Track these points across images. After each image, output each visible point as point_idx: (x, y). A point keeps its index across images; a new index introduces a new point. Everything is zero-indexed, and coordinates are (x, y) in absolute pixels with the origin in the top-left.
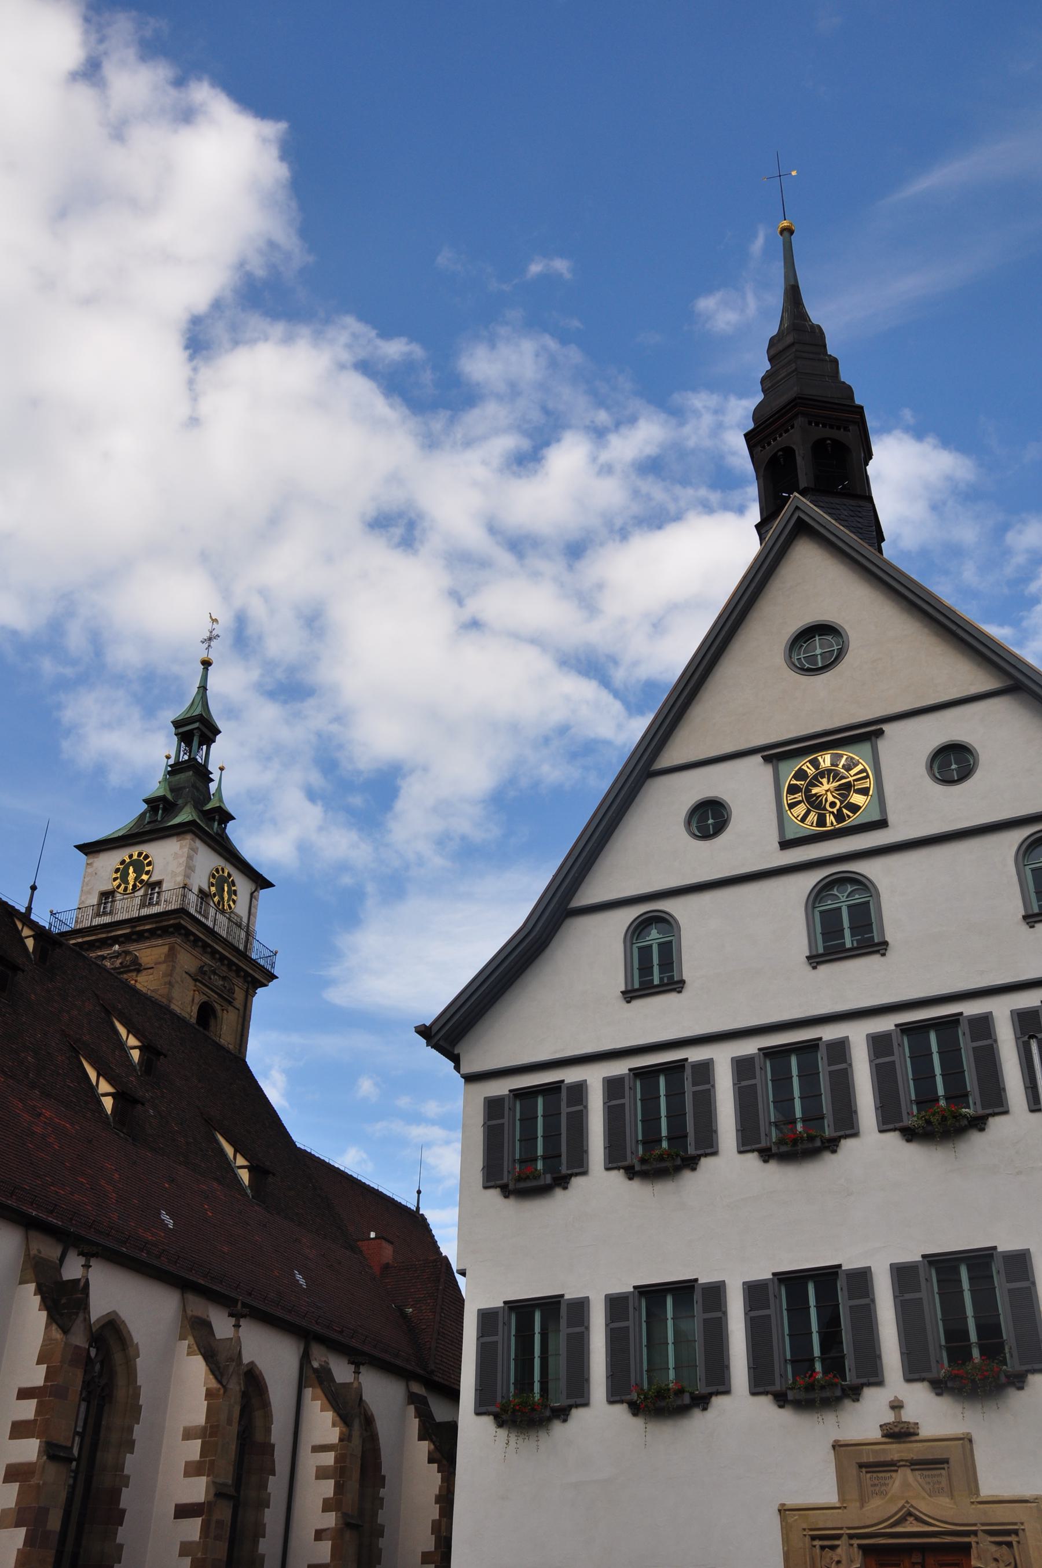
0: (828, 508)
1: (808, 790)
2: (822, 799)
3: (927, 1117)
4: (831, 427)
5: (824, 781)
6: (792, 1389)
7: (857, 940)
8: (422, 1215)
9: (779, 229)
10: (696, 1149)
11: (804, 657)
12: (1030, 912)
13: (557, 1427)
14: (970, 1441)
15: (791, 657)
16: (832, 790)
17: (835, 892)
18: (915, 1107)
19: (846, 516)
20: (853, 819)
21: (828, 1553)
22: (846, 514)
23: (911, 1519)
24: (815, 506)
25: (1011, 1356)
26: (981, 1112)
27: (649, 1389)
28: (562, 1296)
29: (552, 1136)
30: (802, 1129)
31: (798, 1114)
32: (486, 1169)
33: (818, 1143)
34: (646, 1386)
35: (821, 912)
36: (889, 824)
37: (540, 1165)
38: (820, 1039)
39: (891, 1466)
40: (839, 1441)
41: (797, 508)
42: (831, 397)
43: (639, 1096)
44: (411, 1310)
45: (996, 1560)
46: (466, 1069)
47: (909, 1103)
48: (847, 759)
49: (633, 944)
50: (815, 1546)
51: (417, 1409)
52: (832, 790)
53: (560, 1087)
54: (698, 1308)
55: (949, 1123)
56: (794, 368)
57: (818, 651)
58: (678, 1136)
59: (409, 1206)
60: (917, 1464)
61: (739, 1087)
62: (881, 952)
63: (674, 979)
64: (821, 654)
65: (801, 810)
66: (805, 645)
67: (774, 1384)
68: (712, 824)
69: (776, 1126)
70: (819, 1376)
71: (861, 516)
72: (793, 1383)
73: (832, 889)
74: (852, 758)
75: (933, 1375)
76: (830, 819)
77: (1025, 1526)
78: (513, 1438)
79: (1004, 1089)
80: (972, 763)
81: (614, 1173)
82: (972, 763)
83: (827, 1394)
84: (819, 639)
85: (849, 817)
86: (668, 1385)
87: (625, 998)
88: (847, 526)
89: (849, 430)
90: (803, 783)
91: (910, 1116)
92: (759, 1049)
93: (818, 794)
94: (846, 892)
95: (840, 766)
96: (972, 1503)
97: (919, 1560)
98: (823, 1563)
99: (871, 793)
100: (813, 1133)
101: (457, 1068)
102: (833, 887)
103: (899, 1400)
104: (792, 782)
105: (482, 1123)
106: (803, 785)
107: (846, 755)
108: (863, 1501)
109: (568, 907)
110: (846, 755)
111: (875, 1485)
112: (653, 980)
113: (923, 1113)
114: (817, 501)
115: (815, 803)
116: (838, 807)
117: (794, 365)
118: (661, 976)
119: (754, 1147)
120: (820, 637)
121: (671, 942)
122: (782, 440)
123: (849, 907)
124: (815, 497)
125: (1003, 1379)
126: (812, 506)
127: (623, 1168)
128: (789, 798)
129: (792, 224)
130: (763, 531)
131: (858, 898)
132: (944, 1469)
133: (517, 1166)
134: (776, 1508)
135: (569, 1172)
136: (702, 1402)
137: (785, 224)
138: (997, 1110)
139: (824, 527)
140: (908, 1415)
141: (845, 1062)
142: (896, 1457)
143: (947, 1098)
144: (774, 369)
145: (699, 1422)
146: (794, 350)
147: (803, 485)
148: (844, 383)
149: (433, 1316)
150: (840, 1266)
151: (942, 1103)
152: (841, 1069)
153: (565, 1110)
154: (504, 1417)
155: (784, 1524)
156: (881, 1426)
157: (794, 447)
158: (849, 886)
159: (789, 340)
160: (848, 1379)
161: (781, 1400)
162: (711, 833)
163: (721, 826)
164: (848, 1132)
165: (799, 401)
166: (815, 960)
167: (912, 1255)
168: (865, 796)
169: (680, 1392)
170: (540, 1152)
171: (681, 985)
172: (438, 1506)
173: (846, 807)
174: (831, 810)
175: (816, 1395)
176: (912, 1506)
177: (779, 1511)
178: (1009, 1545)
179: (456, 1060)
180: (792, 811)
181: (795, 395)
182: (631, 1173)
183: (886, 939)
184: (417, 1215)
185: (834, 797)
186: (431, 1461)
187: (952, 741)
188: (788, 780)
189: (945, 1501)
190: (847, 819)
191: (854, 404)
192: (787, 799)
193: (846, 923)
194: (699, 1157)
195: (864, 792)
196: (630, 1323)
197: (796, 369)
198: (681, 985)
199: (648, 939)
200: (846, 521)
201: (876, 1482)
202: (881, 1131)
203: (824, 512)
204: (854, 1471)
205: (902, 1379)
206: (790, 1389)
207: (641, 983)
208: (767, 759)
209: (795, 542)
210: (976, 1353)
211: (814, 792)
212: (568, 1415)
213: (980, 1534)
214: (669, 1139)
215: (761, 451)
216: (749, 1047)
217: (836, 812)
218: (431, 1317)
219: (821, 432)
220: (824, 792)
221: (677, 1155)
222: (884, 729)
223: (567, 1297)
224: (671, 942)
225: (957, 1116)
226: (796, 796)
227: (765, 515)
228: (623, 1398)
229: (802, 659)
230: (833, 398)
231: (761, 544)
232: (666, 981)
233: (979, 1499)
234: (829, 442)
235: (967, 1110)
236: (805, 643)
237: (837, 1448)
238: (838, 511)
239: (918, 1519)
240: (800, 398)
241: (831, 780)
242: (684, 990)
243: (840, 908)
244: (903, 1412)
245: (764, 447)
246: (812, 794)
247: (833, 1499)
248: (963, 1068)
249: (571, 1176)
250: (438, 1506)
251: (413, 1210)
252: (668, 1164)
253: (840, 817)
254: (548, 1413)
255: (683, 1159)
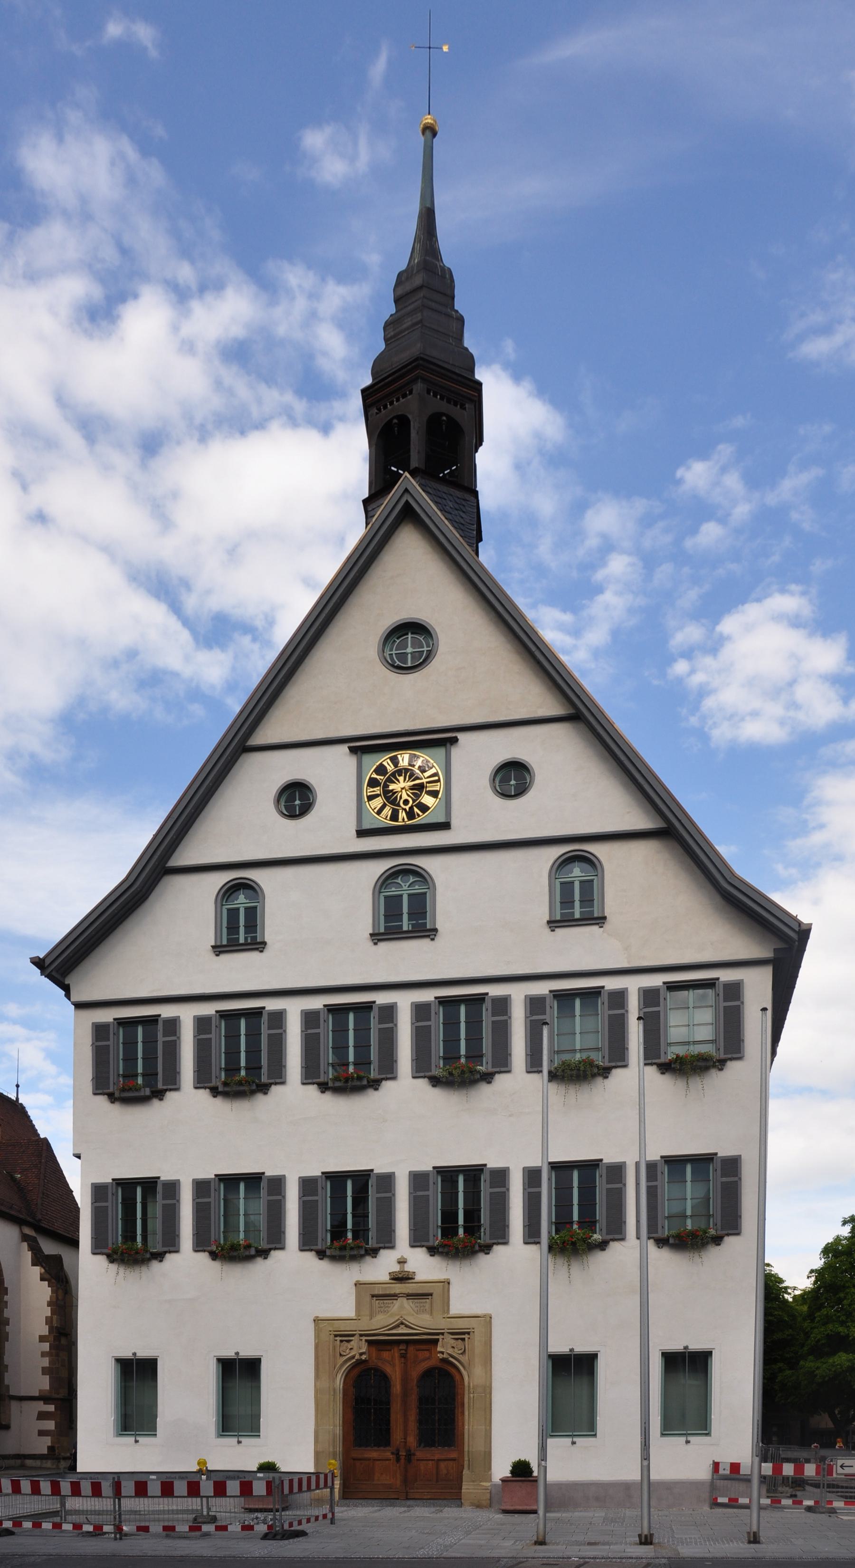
0: (435, 496)
1: (386, 786)
2: (397, 796)
3: (450, 1070)
4: (449, 401)
5: (401, 779)
6: (330, 1248)
7: (412, 924)
8: (21, 1104)
9: (422, 126)
10: (268, 1079)
11: (396, 654)
12: (553, 919)
13: (155, 1265)
14: (449, 1283)
15: (383, 652)
16: (407, 788)
17: (399, 881)
18: (441, 1062)
19: (451, 507)
20: (422, 818)
21: (345, 1344)
22: (452, 506)
23: (403, 1326)
24: (424, 491)
25: (485, 1234)
26: (491, 1070)
27: (225, 1244)
28: (159, 1178)
29: (151, 1059)
30: (353, 1071)
31: (351, 1058)
32: (95, 1080)
33: (365, 1082)
34: (222, 1242)
35: (386, 897)
36: (452, 827)
37: (140, 1080)
38: (374, 1002)
39: (395, 1296)
40: (359, 1281)
41: (406, 490)
42: (452, 365)
43: (223, 1033)
44: (19, 1176)
45: (453, 1347)
46: (76, 997)
47: (437, 1058)
48: (423, 761)
49: (222, 905)
50: (336, 1340)
51: (29, 1245)
52: (407, 788)
53: (157, 1020)
54: (263, 1192)
55: (466, 1076)
56: (419, 318)
57: (409, 650)
58: (254, 1067)
59: (10, 1096)
60: (409, 1296)
61: (306, 1034)
62: (432, 937)
63: (257, 939)
64: (411, 653)
65: (378, 803)
66: (398, 641)
67: (317, 1245)
68: (298, 805)
69: (333, 1066)
70: (350, 1241)
71: (464, 510)
72: (331, 1245)
73: (397, 878)
74: (428, 761)
75: (430, 1244)
76: (402, 815)
77: (475, 1330)
78: (122, 1270)
79: (510, 1055)
80: (528, 781)
81: (202, 1091)
82: (528, 781)
83: (355, 1252)
84: (412, 637)
85: (419, 816)
86: (239, 1242)
87: (215, 952)
88: (451, 520)
89: (465, 409)
90: (382, 778)
91: (437, 1069)
92: (325, 1006)
93: (394, 791)
94: (408, 882)
95: (417, 767)
96: (444, 1318)
97: (404, 1348)
98: (341, 1349)
99: (440, 796)
100: (362, 1074)
101: (68, 995)
102: (398, 877)
103: (404, 1258)
104: (372, 776)
105: (91, 1043)
106: (382, 780)
107: (423, 757)
108: (371, 1316)
109: (167, 865)
110: (423, 757)
111: (381, 1307)
112: (238, 938)
113: (448, 1067)
114: (425, 486)
115: (391, 798)
116: (410, 805)
117: (419, 314)
118: (246, 935)
119: (315, 1081)
120: (413, 636)
121: (256, 907)
122: (398, 406)
123: (409, 895)
124: (423, 480)
125: (477, 1248)
126: (421, 491)
127: (209, 1088)
128: (368, 791)
129: (435, 122)
130: (370, 508)
131: (418, 889)
132: (428, 1299)
133: (121, 1079)
134: (312, 1319)
135: (165, 1087)
136: (264, 1253)
137: (428, 120)
138: (503, 1069)
139: (430, 518)
140: (408, 1268)
141: (392, 1022)
142: (397, 1291)
143: (467, 1057)
144: (399, 314)
145: (260, 1266)
146: (422, 295)
147: (414, 463)
148: (466, 349)
149: (37, 1182)
150: (372, 1170)
151: (463, 1060)
152: (388, 1028)
153: (161, 1039)
154: (115, 1257)
155: (317, 1328)
156: (390, 1273)
157: (410, 417)
158: (411, 877)
159: (418, 281)
160: (370, 1244)
161: (321, 1254)
162: (297, 813)
163: (306, 808)
164: (389, 1076)
165: (421, 362)
166: (377, 937)
167: (426, 1166)
168: (435, 798)
169: (248, 1247)
170: (140, 1070)
171: (263, 946)
172: (50, 1308)
173: (417, 806)
174: (404, 807)
175: (347, 1253)
176: (404, 1319)
177: (314, 1320)
178: (463, 1339)
179: (67, 989)
180: (370, 802)
181: (418, 353)
182: (215, 1092)
183: (437, 927)
184: (17, 1104)
185: (408, 795)
186: (42, 1279)
187: (515, 758)
188: (370, 773)
189: (426, 1317)
190: (417, 817)
191: (472, 378)
192: (367, 791)
193: (405, 909)
194: (271, 1084)
195: (434, 794)
196: (211, 1200)
197: (421, 321)
198: (263, 946)
199: (236, 902)
200: (451, 513)
201: (382, 1305)
202: (414, 1077)
203: (431, 500)
204: (368, 1298)
205: (408, 1245)
206: (328, 1248)
207: (228, 940)
208: (353, 750)
209: (400, 528)
210: (461, 1231)
211: (391, 788)
212: (163, 1258)
213: (445, 1334)
214: (247, 1069)
215: (377, 413)
216: (316, 1003)
217: (408, 810)
218: (36, 1182)
219: (438, 405)
220: (400, 790)
221: (253, 1082)
222: (458, 737)
223: (162, 1179)
224: (256, 907)
225: (472, 1072)
226: (375, 789)
227: (373, 492)
228: (205, 1248)
229: (394, 656)
230: (455, 366)
231: (367, 524)
232: (249, 941)
233: (448, 1316)
234: (444, 418)
235: (481, 1067)
236: (398, 638)
237: (357, 1285)
238: (444, 501)
239: (407, 1326)
240: (422, 359)
241: (407, 779)
242: (265, 950)
243: (401, 896)
244: (406, 1265)
245: (379, 410)
246: (389, 790)
247: (352, 1314)
248: (482, 1035)
249: (166, 1090)
250: (50, 1308)
251: (13, 1100)
252: (246, 1088)
253: (411, 815)
254: (148, 1256)
255: (258, 1085)
